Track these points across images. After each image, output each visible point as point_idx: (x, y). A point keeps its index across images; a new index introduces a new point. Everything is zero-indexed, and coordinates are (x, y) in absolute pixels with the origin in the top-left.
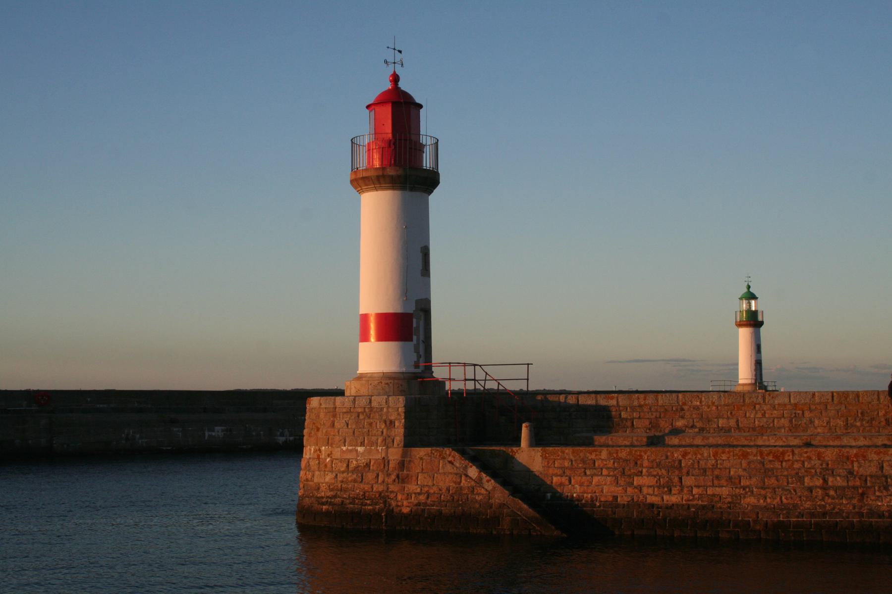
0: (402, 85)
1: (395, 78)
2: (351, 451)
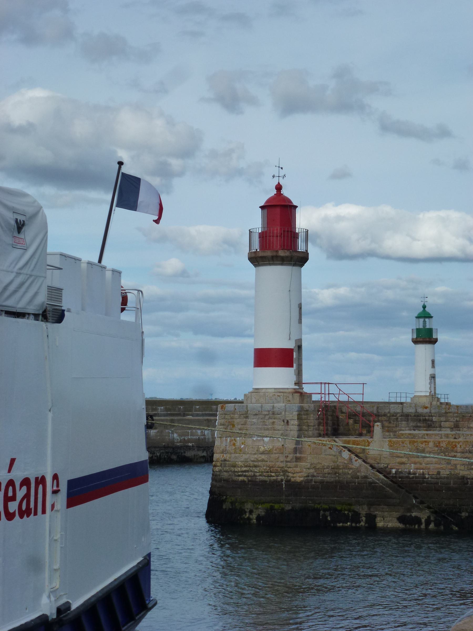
0: (284, 192)
1: (279, 188)
2: (260, 440)
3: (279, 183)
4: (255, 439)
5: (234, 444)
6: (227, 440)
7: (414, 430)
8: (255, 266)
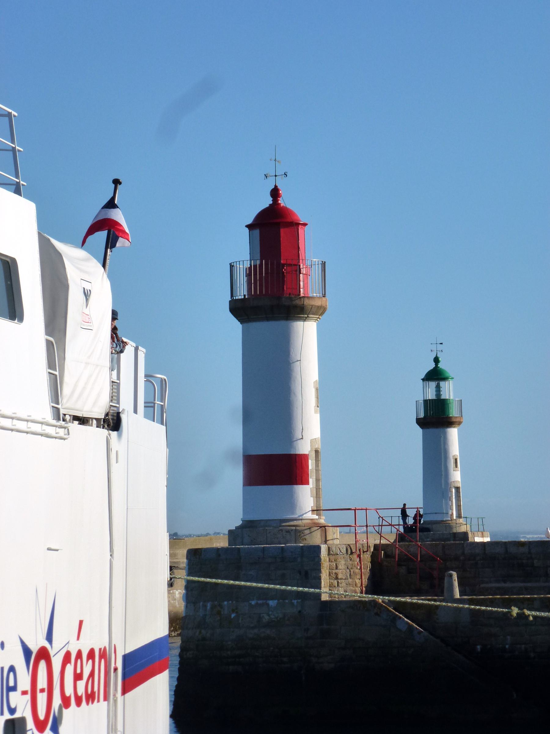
1: (275, 193)
3: (276, 186)
4: (253, 603)
5: (219, 613)
6: (205, 606)
7: (505, 582)
8: (242, 321)
